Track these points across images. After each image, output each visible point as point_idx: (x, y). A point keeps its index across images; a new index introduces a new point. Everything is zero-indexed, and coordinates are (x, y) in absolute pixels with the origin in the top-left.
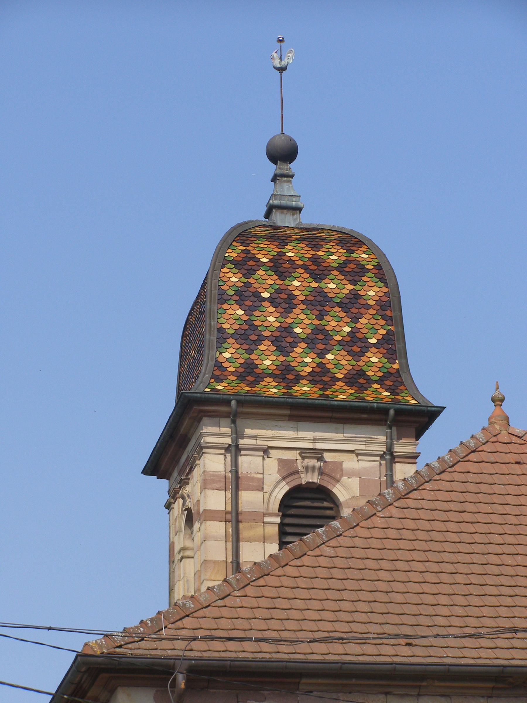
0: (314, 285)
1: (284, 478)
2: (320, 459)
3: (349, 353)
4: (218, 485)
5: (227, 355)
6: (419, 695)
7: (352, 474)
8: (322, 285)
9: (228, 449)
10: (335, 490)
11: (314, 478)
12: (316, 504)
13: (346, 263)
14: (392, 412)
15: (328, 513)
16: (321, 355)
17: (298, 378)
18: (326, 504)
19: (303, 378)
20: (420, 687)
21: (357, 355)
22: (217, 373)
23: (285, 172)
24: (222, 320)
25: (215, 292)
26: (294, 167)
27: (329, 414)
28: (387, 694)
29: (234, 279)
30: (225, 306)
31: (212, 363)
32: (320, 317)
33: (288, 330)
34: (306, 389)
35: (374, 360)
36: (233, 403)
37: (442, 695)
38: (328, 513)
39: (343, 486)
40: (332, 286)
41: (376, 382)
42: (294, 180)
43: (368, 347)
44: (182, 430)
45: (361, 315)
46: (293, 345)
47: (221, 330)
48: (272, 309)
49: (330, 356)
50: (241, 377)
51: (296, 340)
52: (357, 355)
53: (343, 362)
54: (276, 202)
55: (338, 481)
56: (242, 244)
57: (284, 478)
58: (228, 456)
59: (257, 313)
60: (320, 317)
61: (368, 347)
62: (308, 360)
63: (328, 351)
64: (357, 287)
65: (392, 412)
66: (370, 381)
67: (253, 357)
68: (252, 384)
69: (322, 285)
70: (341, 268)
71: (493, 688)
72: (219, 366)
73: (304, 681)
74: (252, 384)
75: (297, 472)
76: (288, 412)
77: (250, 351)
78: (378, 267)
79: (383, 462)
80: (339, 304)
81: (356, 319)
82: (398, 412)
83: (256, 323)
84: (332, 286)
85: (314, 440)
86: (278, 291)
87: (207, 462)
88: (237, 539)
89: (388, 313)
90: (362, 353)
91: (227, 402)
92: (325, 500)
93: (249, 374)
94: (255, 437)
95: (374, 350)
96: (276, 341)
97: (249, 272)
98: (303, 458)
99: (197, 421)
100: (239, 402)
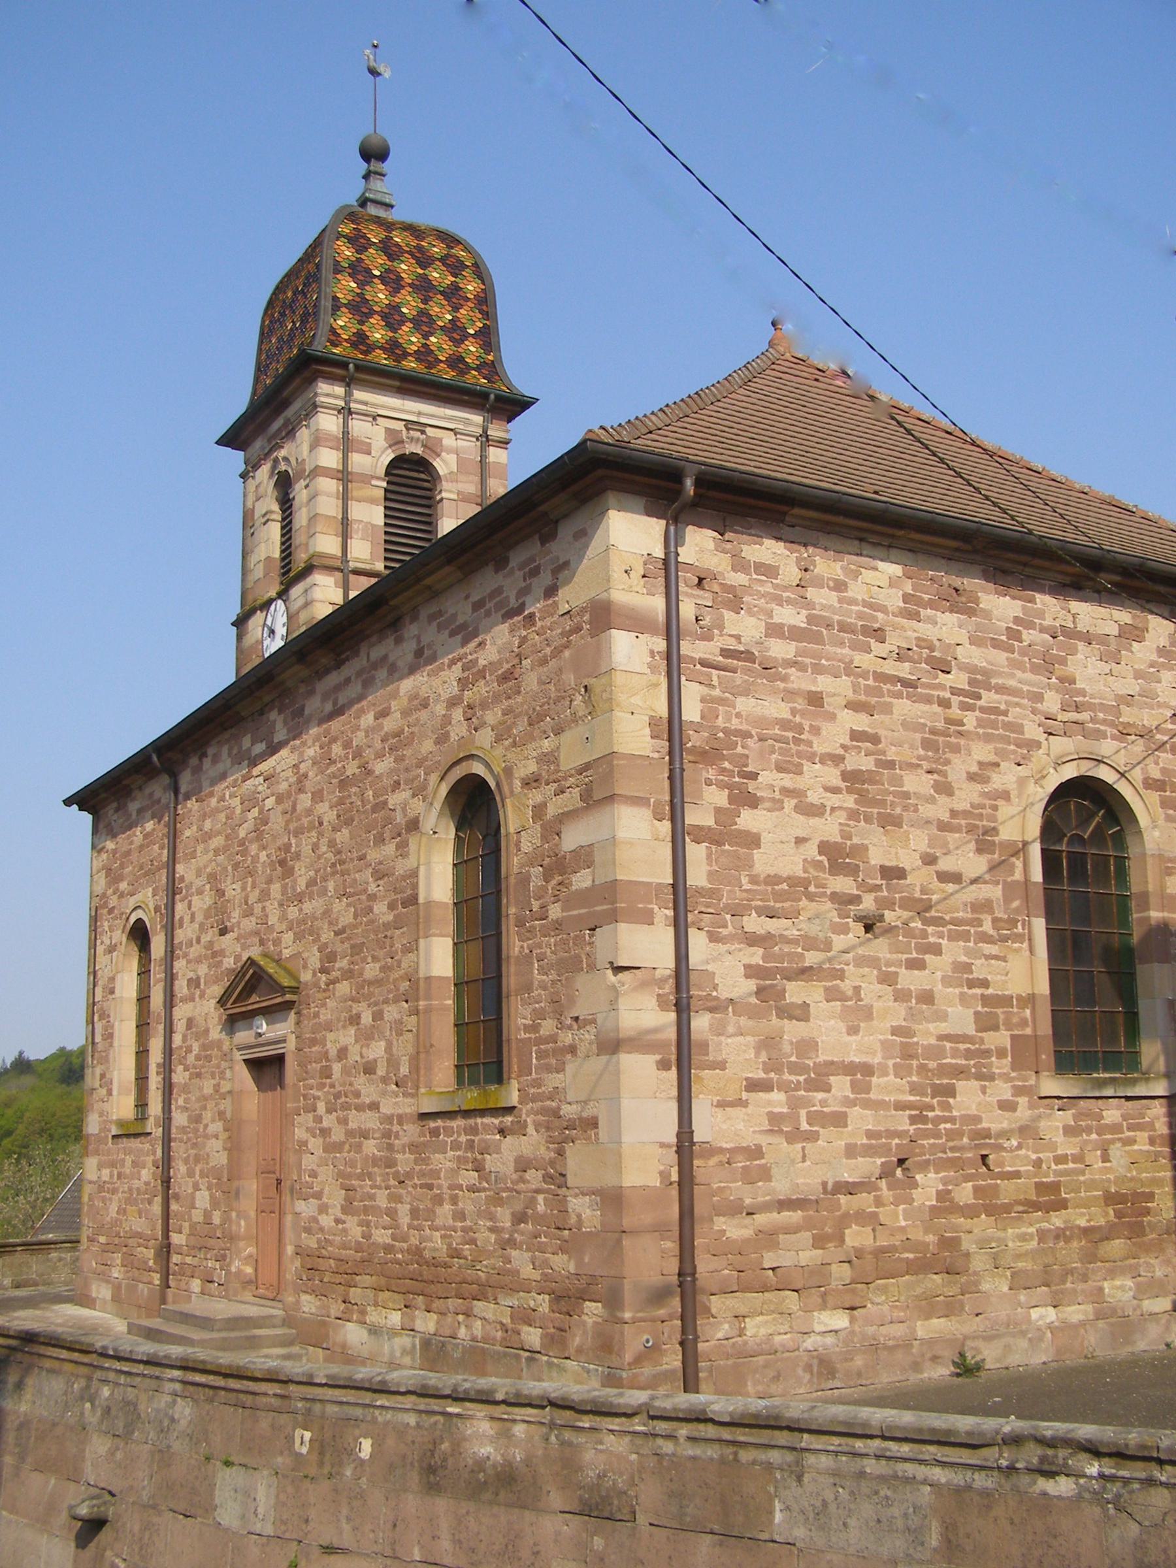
0: (420, 271)
1: (390, 446)
2: (423, 432)
3: (451, 339)
4: (330, 444)
5: (341, 323)
6: (890, 546)
7: (449, 452)
8: (427, 272)
9: (340, 411)
10: (435, 464)
11: (418, 450)
12: (415, 475)
13: (448, 256)
14: (492, 396)
15: (426, 485)
16: (426, 336)
17: (405, 355)
18: (422, 476)
19: (410, 355)
20: (893, 536)
21: (458, 342)
22: (332, 338)
23: (379, 170)
24: (335, 289)
25: (331, 262)
26: (385, 167)
27: (433, 391)
28: (861, 540)
29: (347, 253)
30: (339, 276)
31: (327, 328)
32: (425, 302)
33: (396, 308)
34: (413, 365)
35: (472, 349)
36: (351, 366)
37: (910, 550)
38: (426, 485)
39: (443, 460)
40: (436, 275)
41: (474, 369)
42: (385, 179)
43: (466, 336)
44: (285, 394)
45: (462, 306)
46: (402, 323)
47: (335, 299)
48: (382, 287)
49: (433, 339)
50: (354, 345)
51: (403, 320)
52: (458, 342)
53: (445, 346)
54: (371, 196)
55: (439, 455)
56: (353, 222)
57: (390, 446)
58: (341, 416)
59: (367, 288)
60: (425, 302)
61: (466, 336)
62: (414, 339)
63: (432, 334)
64: (458, 280)
65: (492, 396)
66: (468, 368)
67: (364, 328)
68: (366, 353)
69: (427, 272)
70: (443, 260)
71: (957, 549)
72: (333, 331)
73: (797, 511)
74: (366, 353)
75: (403, 442)
76: (397, 383)
77: (361, 323)
78: (476, 265)
79: (479, 443)
80: (442, 293)
81: (456, 309)
82: (499, 398)
83: (368, 297)
84: (436, 275)
85: (419, 414)
86: (388, 271)
87: (321, 420)
88: (345, 498)
89: (484, 308)
90: (462, 341)
91: (345, 365)
92: (422, 472)
93: (362, 343)
94: (366, 403)
95: (471, 339)
96: (385, 316)
97: (362, 249)
98: (408, 429)
99: (311, 381)
100: (357, 367)
